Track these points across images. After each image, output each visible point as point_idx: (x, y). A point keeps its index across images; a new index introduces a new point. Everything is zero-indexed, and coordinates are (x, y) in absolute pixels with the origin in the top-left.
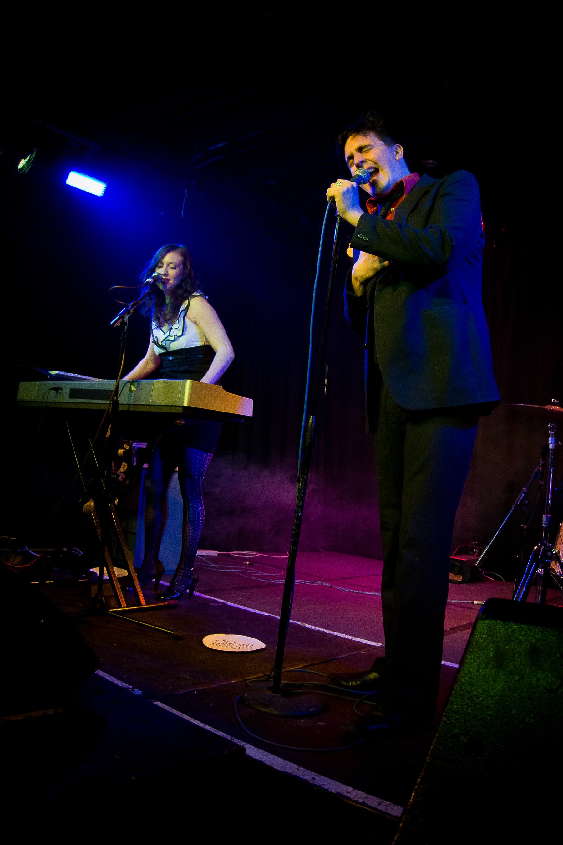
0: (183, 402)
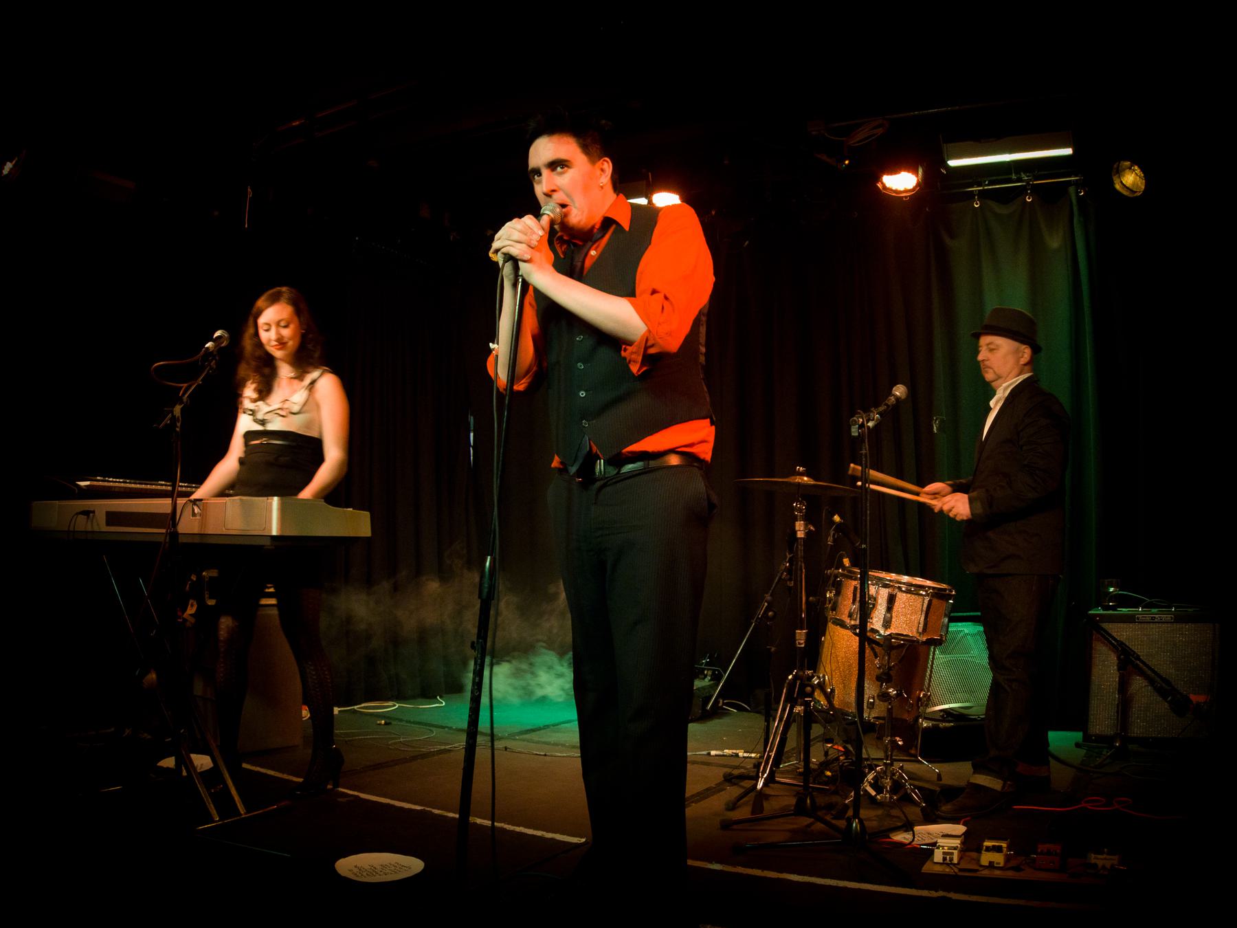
0: (271, 530)
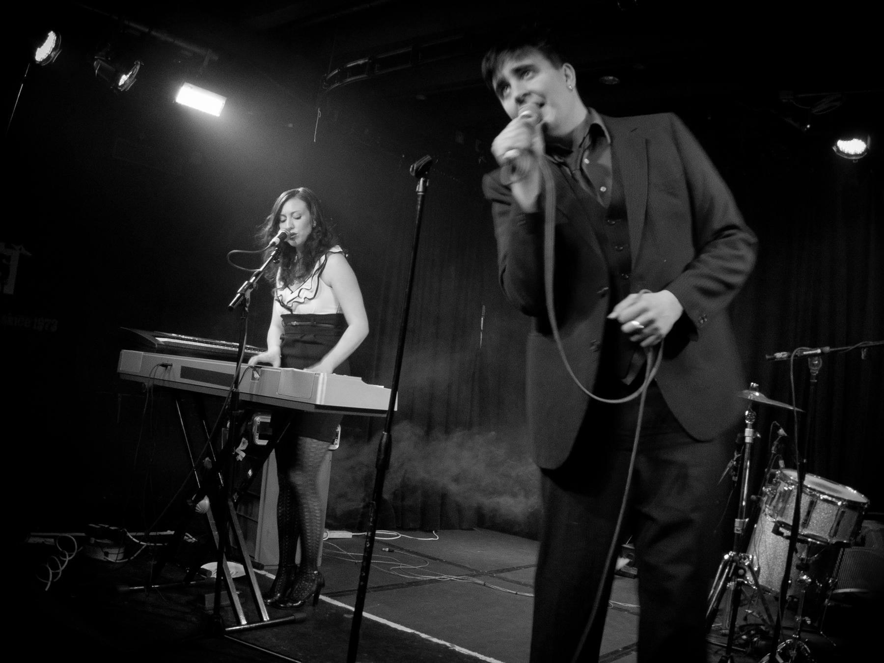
0: (315, 400)
